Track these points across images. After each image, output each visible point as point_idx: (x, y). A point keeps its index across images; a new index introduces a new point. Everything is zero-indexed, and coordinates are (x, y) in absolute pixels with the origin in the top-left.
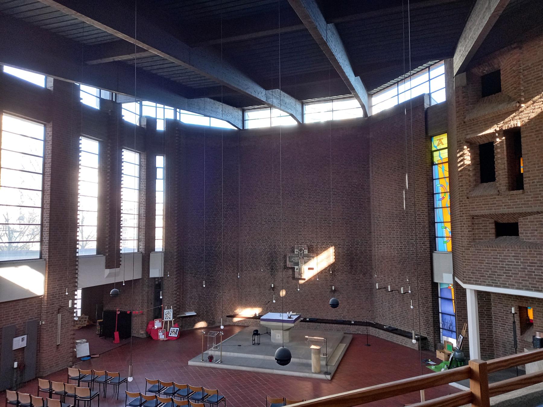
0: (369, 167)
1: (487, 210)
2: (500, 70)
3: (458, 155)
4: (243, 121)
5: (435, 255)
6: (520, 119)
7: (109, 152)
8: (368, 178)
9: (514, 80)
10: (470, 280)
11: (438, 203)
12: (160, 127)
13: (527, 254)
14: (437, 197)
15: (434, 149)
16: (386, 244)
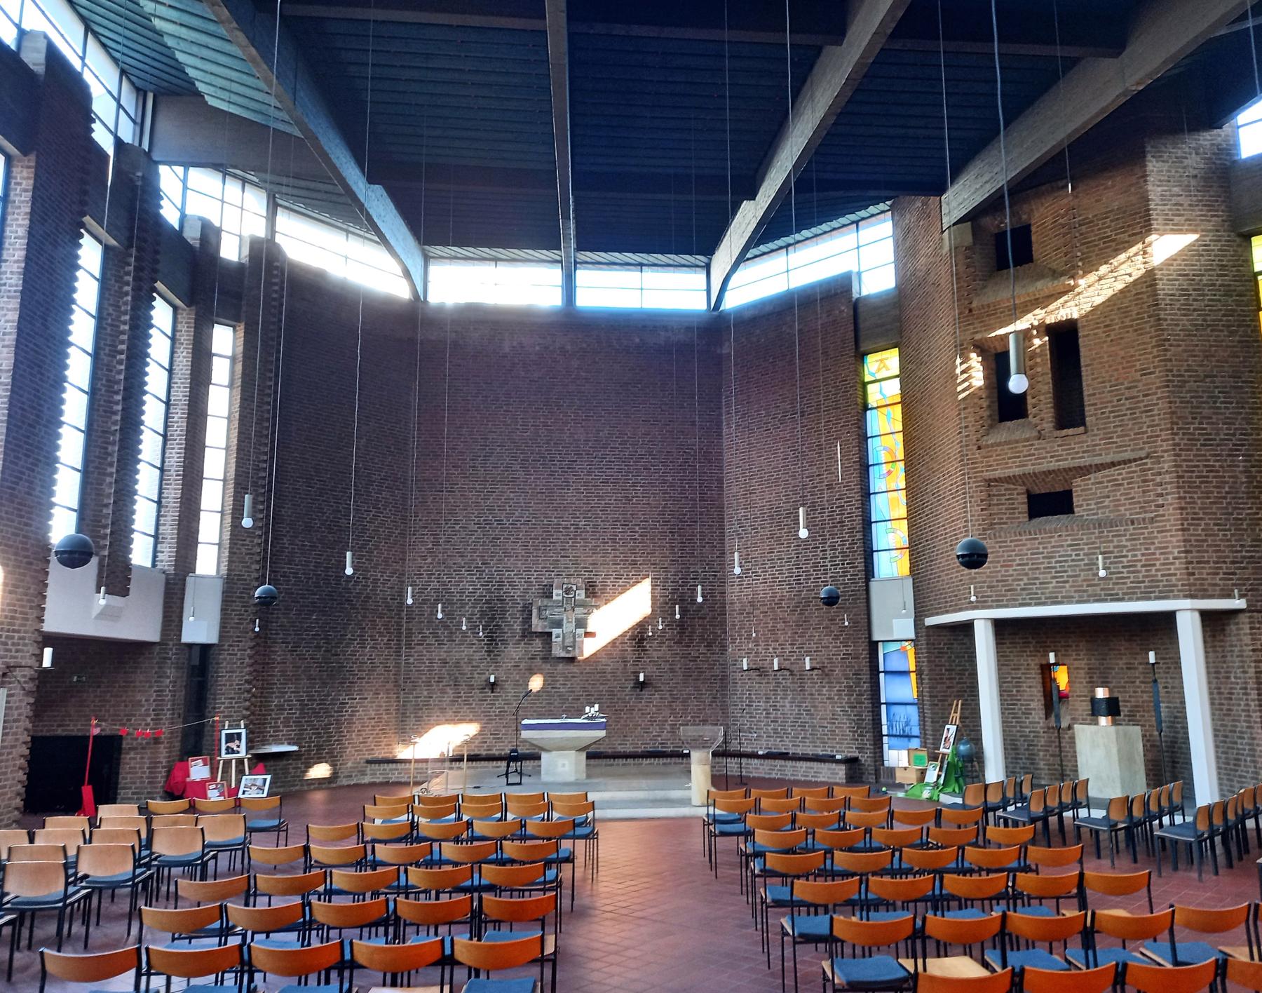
0: (721, 415)
2: (1030, 225)
5: (874, 586)
8: (720, 435)
11: (877, 484)
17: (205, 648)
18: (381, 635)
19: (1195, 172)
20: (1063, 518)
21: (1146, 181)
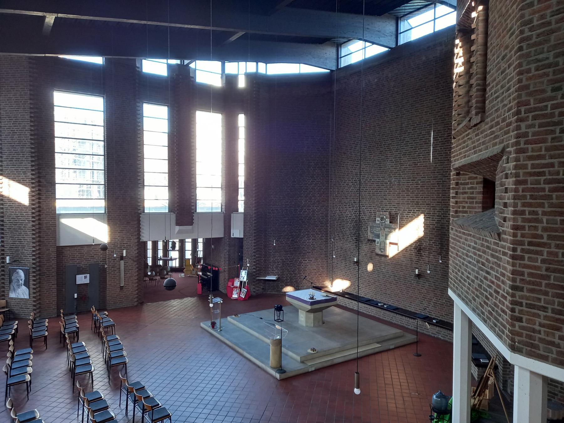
12: (242, 84)
17: (240, 240)
18: (317, 234)
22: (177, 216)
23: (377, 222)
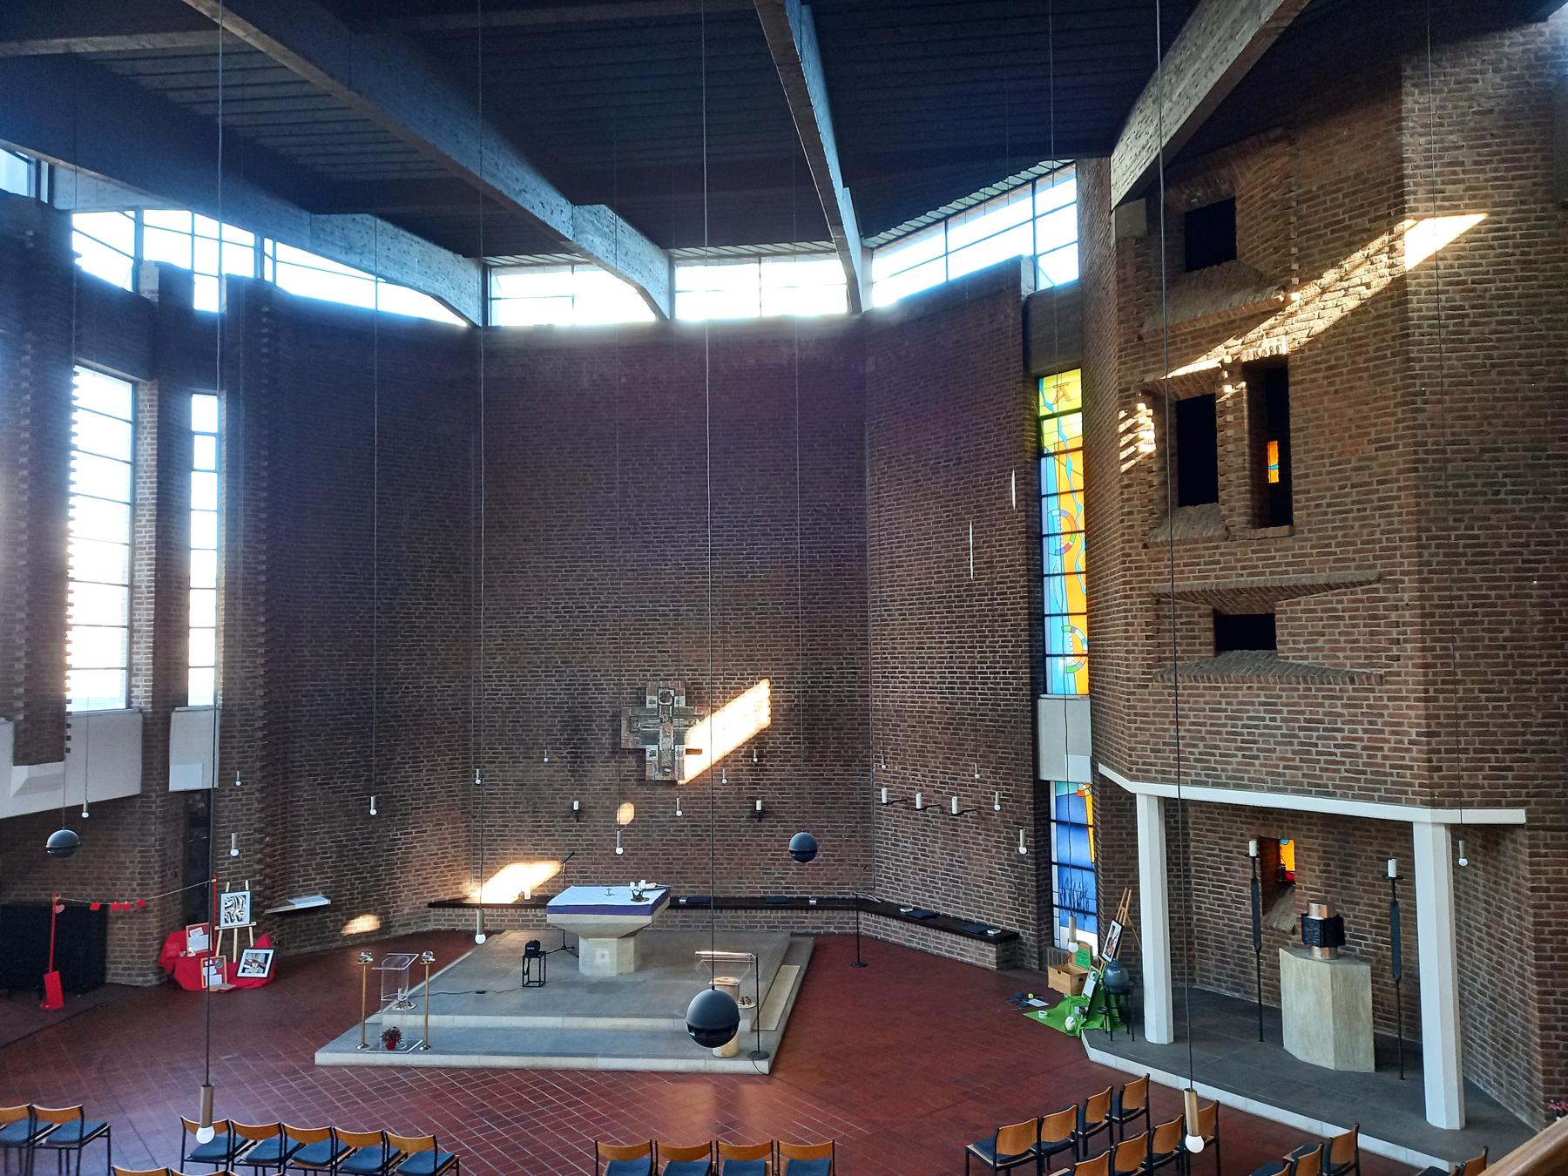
0: (862, 457)
1: (1196, 578)
2: (1234, 199)
3: (1122, 428)
4: (485, 299)
5: (1043, 704)
6: (1287, 333)
7: (26, 371)
8: (862, 485)
9: (1273, 227)
10: (1147, 771)
11: (1052, 563)
13: (1300, 697)
14: (1050, 545)
15: (1043, 411)
16: (909, 677)
18: (441, 753)
19: (1487, 105)
20: (1261, 653)
21: (1400, 129)
22: (17, 734)
23: (648, 706)
